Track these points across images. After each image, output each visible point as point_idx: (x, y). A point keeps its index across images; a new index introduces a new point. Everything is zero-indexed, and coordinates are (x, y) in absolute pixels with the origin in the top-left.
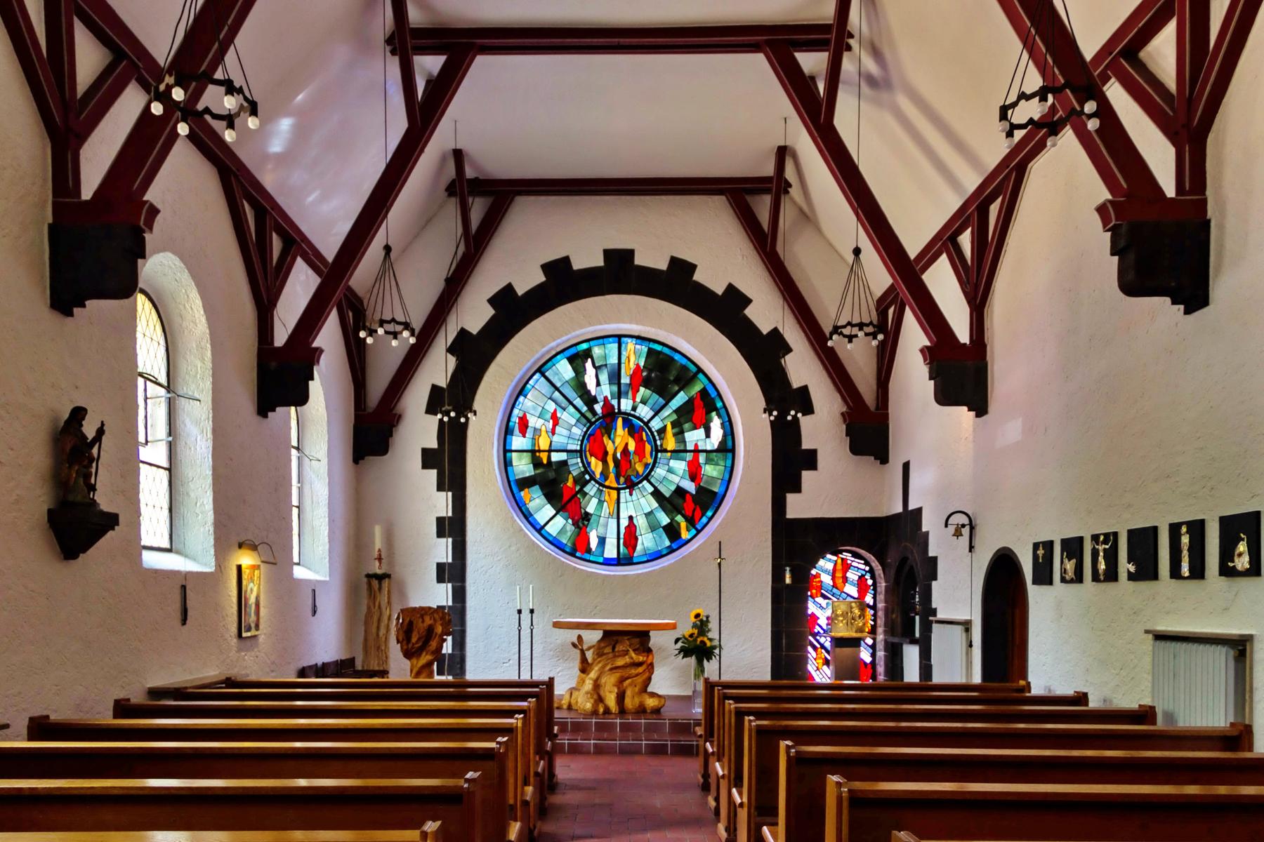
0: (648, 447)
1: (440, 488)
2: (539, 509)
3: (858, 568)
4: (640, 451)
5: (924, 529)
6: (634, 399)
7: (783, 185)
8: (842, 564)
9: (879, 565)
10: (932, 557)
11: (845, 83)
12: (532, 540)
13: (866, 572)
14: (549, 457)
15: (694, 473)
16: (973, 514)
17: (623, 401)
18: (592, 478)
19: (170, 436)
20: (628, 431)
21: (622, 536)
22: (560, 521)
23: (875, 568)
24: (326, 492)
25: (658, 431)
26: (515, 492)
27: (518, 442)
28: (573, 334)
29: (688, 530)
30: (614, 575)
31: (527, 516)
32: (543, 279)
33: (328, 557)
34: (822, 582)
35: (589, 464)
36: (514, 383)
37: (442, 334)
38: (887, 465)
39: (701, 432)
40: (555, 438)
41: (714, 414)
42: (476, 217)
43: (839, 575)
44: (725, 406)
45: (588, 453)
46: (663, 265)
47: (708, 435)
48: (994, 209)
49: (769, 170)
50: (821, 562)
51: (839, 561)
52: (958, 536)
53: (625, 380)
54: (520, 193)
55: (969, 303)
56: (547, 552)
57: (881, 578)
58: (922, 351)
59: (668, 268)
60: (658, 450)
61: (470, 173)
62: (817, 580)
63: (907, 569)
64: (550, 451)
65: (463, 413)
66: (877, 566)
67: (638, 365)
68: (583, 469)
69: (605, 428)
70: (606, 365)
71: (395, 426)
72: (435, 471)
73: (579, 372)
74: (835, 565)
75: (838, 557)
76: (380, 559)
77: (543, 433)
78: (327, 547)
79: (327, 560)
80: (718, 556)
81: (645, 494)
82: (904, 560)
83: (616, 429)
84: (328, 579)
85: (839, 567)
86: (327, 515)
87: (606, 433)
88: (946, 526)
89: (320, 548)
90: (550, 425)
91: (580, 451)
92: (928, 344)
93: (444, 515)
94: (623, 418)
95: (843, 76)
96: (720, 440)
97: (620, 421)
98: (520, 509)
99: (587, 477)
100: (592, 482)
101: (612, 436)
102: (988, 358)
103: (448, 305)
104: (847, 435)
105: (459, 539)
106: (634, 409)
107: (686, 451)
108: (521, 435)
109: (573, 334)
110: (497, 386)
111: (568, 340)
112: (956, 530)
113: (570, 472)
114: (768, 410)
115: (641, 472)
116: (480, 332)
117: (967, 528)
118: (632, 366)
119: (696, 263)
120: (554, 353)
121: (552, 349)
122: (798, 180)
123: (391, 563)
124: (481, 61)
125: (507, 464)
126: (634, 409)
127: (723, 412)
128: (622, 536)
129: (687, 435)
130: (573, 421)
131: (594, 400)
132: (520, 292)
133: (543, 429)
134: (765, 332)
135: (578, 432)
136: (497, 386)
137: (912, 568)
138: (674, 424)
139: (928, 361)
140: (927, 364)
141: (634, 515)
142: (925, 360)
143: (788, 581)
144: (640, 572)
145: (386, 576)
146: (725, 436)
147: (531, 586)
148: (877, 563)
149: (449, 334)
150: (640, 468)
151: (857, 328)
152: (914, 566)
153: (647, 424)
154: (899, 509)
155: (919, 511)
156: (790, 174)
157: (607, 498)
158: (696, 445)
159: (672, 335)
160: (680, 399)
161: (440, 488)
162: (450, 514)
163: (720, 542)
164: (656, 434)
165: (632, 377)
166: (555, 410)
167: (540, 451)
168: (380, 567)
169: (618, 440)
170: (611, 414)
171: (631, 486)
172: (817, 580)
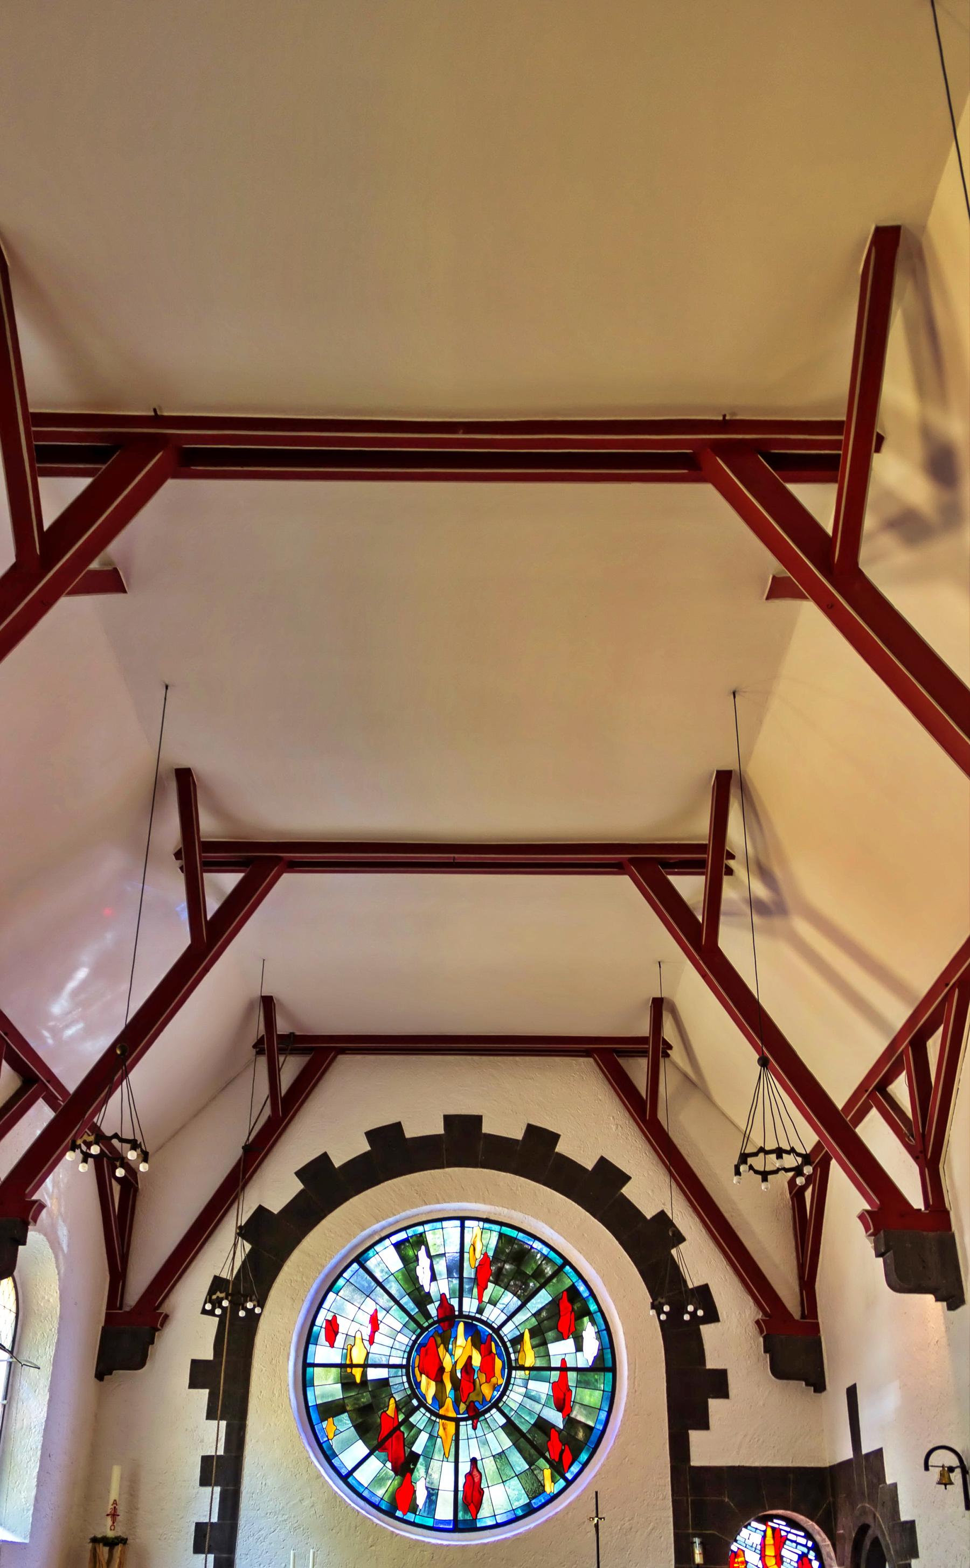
0: (498, 1363)
1: (211, 1414)
2: (348, 1444)
3: (798, 1544)
4: (487, 1368)
5: (889, 1481)
6: (480, 1298)
7: (661, 1046)
8: (774, 1538)
9: (827, 1539)
10: (906, 1522)
11: (730, 914)
12: (333, 1490)
13: (809, 1549)
14: (364, 1374)
15: (562, 1400)
16: (963, 1452)
17: (466, 1301)
18: (422, 1404)
19: (6, 1399)
20: (472, 1340)
21: (461, 1488)
22: (374, 1466)
23: (821, 1544)
24: (43, 1415)
25: (512, 1341)
26: (314, 1423)
27: (322, 1353)
28: (403, 1214)
29: (554, 1481)
30: (448, 1546)
31: (328, 1456)
32: (368, 1148)
33: (32, 1508)
34: (747, 1562)
35: (418, 1384)
36: (322, 1276)
37: (233, 1213)
38: (824, 1394)
39: (569, 1344)
40: (374, 1349)
41: (586, 1319)
42: (287, 1079)
43: (770, 1552)
44: (600, 1310)
45: (417, 1370)
46: (518, 1134)
47: (579, 1348)
48: (934, 1046)
49: (643, 1028)
50: (744, 1533)
51: (769, 1532)
52: (945, 1485)
53: (468, 1272)
54: (343, 1051)
55: (916, 1158)
56: (354, 1508)
57: (831, 1559)
58: (861, 1217)
59: (524, 1138)
60: (511, 1367)
61: (282, 1027)
62: (741, 1559)
63: (867, 1543)
64: (365, 1366)
65: (243, 1305)
66: (824, 1540)
67: (486, 1255)
68: (409, 1392)
69: (440, 1335)
70: (444, 1254)
71: (159, 1330)
72: (207, 1391)
73: (409, 1263)
74: (764, 1537)
75: (767, 1525)
76: (114, 1515)
77: (358, 1341)
78: (34, 1493)
79: (31, 1512)
80: (594, 1514)
81: (493, 1428)
82: (863, 1530)
83: (456, 1338)
84: (27, 1541)
85: (770, 1540)
86: (40, 1447)
87: (443, 1343)
88: (927, 1468)
89: (23, 1494)
90: (367, 1331)
91: (406, 1367)
92: (868, 1207)
93: (211, 1452)
94: (465, 1323)
95: (723, 907)
96: (595, 1354)
97: (461, 1327)
98: (320, 1445)
99: (415, 1402)
100: (422, 1410)
101: (450, 1346)
102: (954, 1228)
103: (244, 1177)
104: (765, 1352)
105: (231, 1488)
106: (480, 1310)
107: (550, 1369)
108: (327, 1344)
109: (403, 1214)
110: (299, 1279)
111: (397, 1222)
112: (942, 1475)
113: (392, 1396)
114: (657, 1307)
115: (488, 1398)
116: (281, 1212)
117: (958, 1471)
118: (479, 1255)
119: (559, 1133)
120: (377, 1238)
121: (375, 1233)
122: (679, 1039)
123: (132, 1522)
124: (287, 880)
125: (305, 1383)
126: (480, 1310)
127: (598, 1317)
128: (461, 1488)
129: (550, 1346)
130: (399, 1326)
131: (428, 1298)
132: (337, 1163)
133: (359, 1335)
134: (649, 1217)
135: (405, 1340)
136: (299, 1279)
137: (876, 1542)
138: (534, 1333)
139: (872, 1231)
140: (870, 1235)
141: (478, 1458)
142: (867, 1230)
143: (698, 1559)
144: (486, 1541)
145: (122, 1541)
146: (601, 1350)
147: (312, 1551)
148: (824, 1536)
149: (245, 1211)
150: (486, 1390)
151: (773, 1156)
152: (880, 1537)
153: (497, 1331)
154: (847, 1453)
155: (878, 1454)
156: (669, 1032)
157: (441, 1432)
158: (563, 1361)
159: (530, 1218)
160: (542, 1299)
161: (211, 1414)
162: (221, 1452)
163: (597, 1493)
164: (509, 1344)
165: (478, 1270)
166: (376, 1311)
167: (352, 1366)
168: (113, 1528)
169: (458, 1352)
170: (449, 1317)
171: (475, 1415)
172: (741, 1559)
